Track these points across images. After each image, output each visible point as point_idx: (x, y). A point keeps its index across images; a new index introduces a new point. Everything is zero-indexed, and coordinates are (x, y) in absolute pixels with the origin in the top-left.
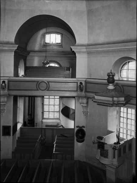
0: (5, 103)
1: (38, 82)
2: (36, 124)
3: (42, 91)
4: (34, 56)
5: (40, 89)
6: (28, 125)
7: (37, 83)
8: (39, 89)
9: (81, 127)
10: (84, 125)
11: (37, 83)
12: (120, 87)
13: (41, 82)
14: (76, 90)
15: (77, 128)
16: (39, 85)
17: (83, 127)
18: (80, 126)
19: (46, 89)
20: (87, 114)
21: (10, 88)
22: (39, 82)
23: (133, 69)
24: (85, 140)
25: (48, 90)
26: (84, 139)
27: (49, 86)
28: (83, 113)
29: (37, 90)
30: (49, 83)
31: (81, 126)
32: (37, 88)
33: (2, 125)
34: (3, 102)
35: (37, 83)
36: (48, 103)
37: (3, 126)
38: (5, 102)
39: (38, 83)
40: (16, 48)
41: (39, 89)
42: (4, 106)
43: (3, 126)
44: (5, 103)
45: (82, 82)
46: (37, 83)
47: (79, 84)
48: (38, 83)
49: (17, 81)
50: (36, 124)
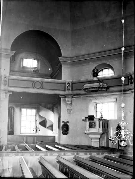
1: (33, 81)
3: (36, 89)
5: (35, 87)
7: (42, 87)
9: (66, 122)
10: (68, 121)
11: (42, 87)
12: (35, 87)
15: (63, 123)
16: (41, 85)
17: (68, 122)
18: (64, 121)
20: (71, 111)
22: (35, 82)
23: (29, 120)
24: (69, 133)
26: (68, 132)
28: (68, 111)
31: (65, 121)
32: (33, 86)
35: (32, 82)
39: (42, 87)
41: (41, 83)
46: (32, 82)
48: (42, 87)
49: (114, 86)
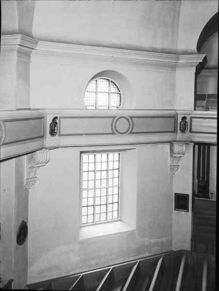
0: (182, 155)
2: (212, 194)
4: (209, 76)
6: (200, 195)
8: (129, 119)
13: (125, 133)
14: (193, 119)
19: (118, 119)
21: (173, 120)
25: (114, 117)
27: (133, 124)
29: (131, 117)
30: (113, 131)
32: (132, 121)
33: (174, 192)
34: (179, 154)
36: (16, 26)
37: (176, 194)
38: (182, 154)
40: (201, 61)
41: (129, 119)
42: (179, 160)
43: (176, 194)
44: (182, 155)
45: (186, 116)
47: (179, 120)
50: (212, 194)
